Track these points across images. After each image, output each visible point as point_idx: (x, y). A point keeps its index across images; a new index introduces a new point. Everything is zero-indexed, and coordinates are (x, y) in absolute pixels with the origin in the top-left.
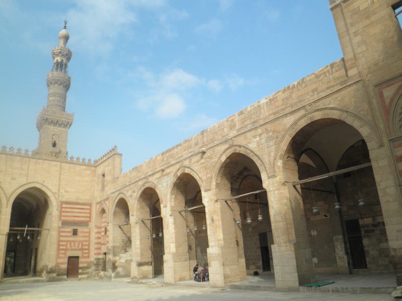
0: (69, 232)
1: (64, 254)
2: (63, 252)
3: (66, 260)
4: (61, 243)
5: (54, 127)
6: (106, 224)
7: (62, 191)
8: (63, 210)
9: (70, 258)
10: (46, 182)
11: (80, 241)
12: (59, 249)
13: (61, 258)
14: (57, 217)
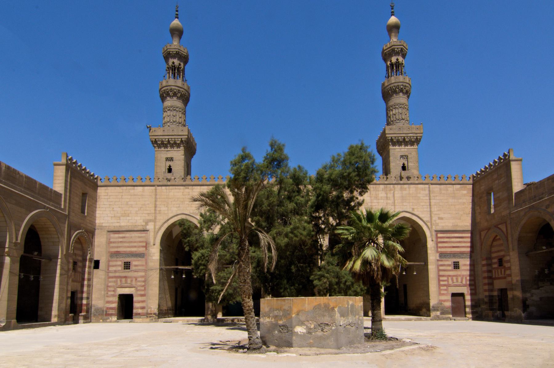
0: (449, 265)
1: (445, 290)
2: (445, 288)
3: (449, 297)
4: (441, 278)
5: (400, 147)
6: (502, 253)
7: (435, 218)
8: (439, 240)
9: (453, 295)
10: (415, 210)
11: (463, 276)
12: (440, 285)
13: (443, 294)
14: (433, 249)
